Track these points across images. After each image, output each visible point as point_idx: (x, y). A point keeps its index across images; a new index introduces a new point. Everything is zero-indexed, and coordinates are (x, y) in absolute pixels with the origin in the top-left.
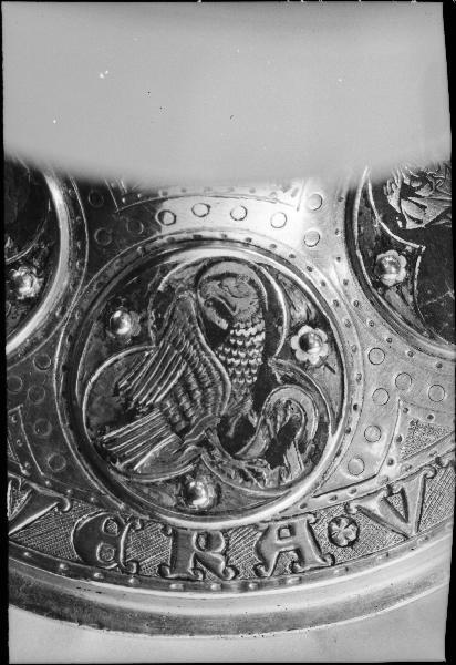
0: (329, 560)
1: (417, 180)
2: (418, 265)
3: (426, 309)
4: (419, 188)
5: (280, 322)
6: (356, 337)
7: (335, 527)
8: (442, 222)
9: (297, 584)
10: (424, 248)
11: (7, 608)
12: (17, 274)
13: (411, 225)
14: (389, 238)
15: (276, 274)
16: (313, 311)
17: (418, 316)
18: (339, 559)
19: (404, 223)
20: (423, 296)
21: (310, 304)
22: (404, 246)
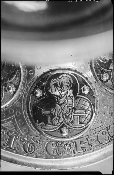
0: (85, 150)
1: (60, 85)
2: (43, 98)
3: (35, 107)
4: (59, 87)
5: (10, 79)
6: (96, 119)
7: (66, 146)
8: (56, 97)
9: (63, 158)
10: (47, 97)
11: (1, 1)
12: (10, 87)
13: (50, 91)
14: (44, 88)
15: (77, 76)
16: (18, 84)
17: (33, 106)
18: (86, 149)
19: (49, 89)
20: (37, 104)
21: (19, 82)
22: (45, 93)
